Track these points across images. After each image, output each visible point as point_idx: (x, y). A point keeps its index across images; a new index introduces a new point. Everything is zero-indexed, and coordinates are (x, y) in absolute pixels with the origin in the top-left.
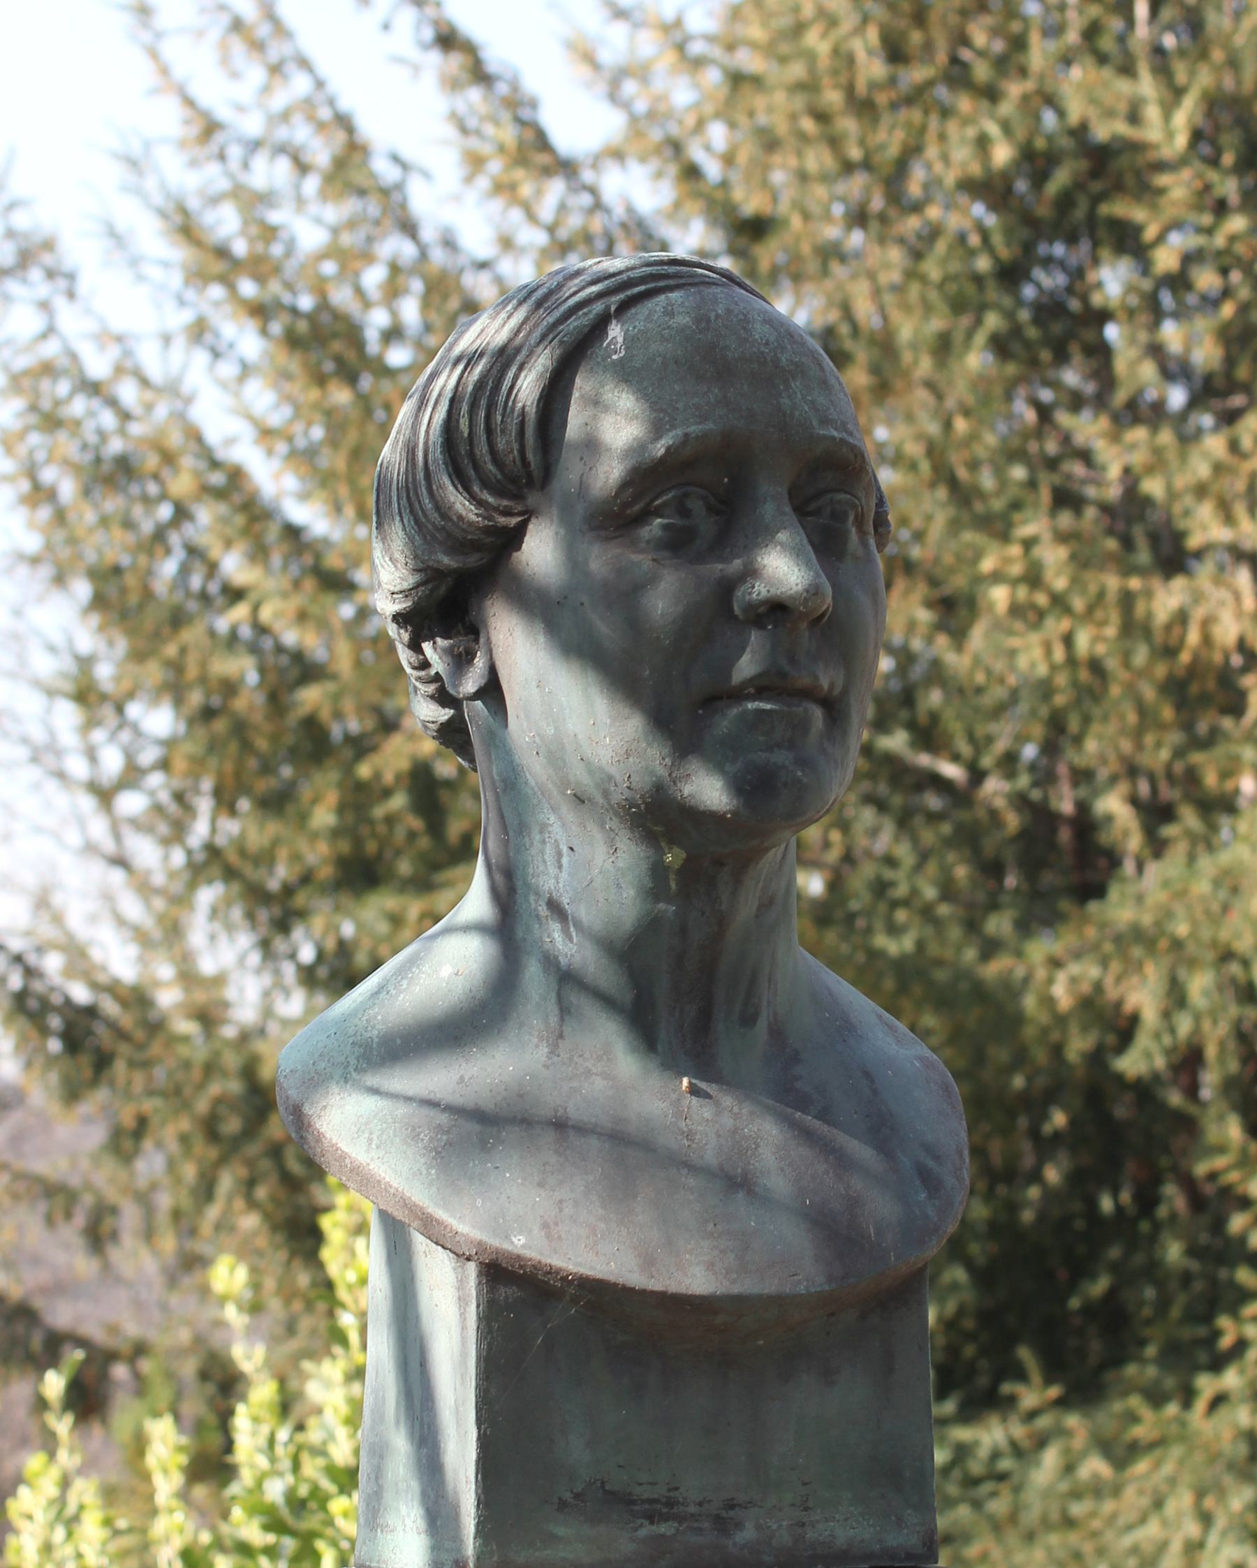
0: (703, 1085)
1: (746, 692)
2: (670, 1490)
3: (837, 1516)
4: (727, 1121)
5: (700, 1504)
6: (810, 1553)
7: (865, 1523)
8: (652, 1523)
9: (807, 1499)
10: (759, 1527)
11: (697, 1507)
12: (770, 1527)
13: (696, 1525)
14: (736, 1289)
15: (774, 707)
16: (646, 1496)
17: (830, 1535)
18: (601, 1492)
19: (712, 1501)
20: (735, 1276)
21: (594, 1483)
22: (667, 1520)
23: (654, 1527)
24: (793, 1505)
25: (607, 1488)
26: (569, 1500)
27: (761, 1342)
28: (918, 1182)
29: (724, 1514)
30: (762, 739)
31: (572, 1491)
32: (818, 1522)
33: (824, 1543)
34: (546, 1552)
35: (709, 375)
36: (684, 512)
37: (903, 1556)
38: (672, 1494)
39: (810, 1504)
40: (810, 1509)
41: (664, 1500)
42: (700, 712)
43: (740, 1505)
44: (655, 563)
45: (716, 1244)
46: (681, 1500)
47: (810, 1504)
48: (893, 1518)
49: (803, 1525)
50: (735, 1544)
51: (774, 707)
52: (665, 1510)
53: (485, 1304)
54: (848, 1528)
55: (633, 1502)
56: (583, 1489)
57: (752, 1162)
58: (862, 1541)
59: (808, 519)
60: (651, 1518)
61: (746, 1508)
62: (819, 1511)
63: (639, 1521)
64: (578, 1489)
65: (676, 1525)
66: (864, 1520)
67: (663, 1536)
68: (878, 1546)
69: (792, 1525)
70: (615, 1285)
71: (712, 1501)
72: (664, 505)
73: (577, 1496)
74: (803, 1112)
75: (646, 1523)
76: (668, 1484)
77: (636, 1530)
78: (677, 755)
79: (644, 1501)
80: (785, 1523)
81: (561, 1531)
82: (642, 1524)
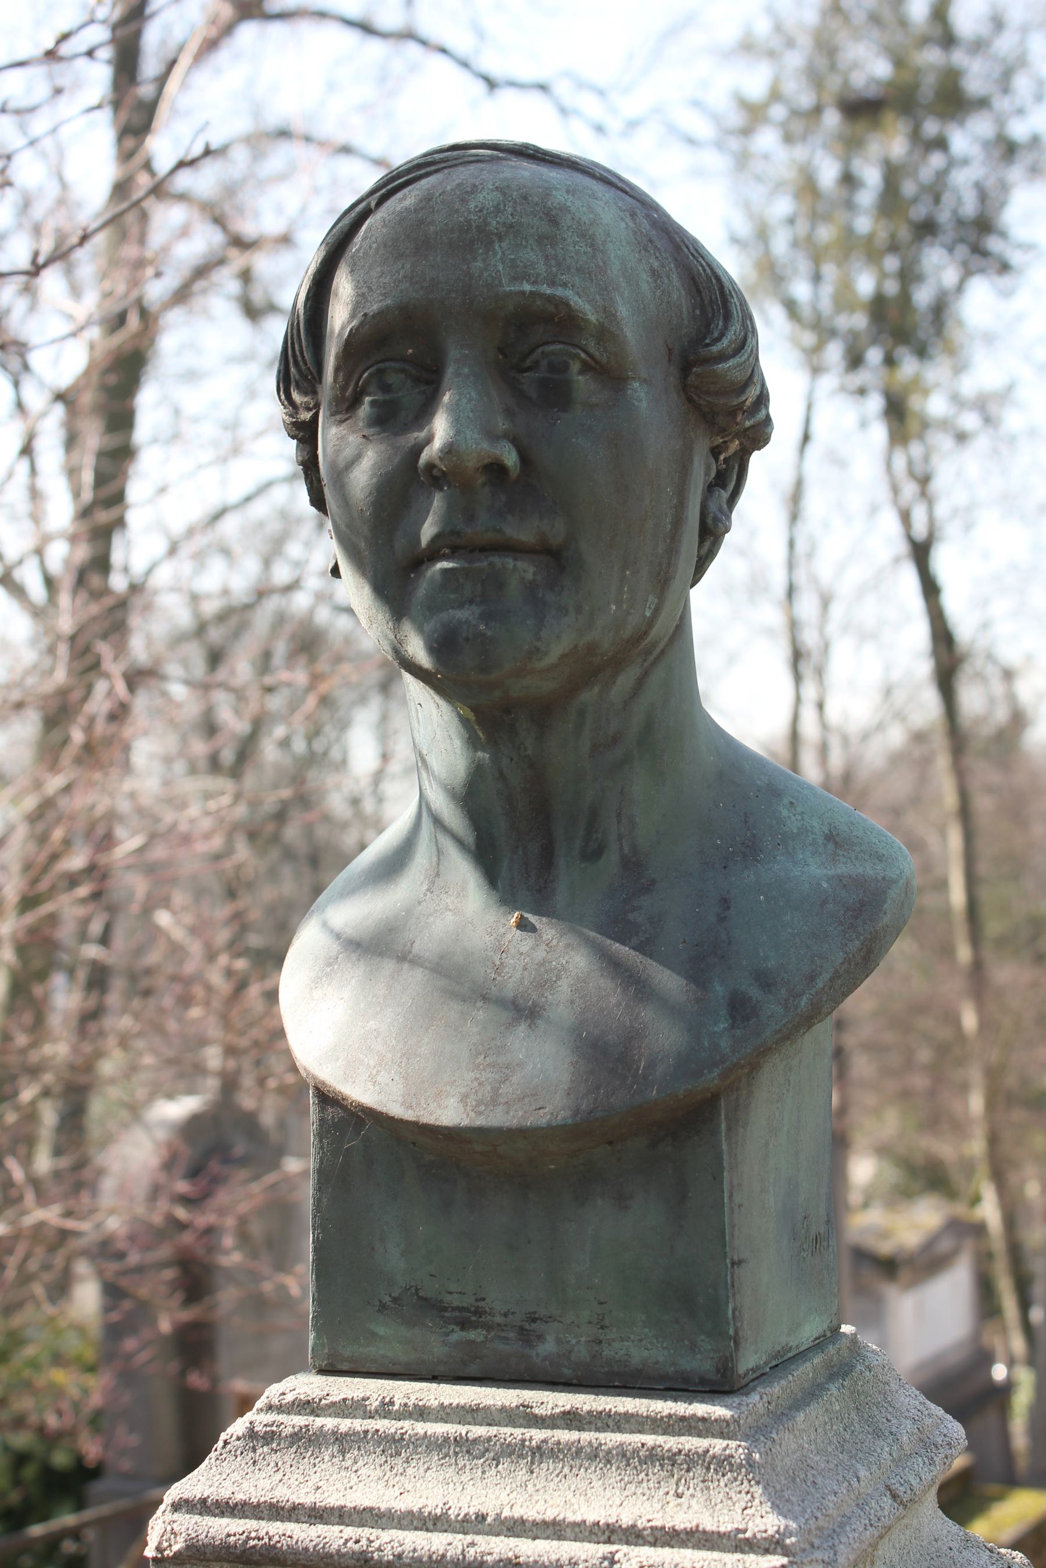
0: (532, 918)
1: (442, 552)
2: (477, 1300)
3: (632, 1337)
4: (540, 954)
5: (505, 1315)
6: (607, 1369)
7: (659, 1345)
8: (463, 1329)
9: (603, 1317)
10: (559, 1341)
11: (502, 1317)
12: (569, 1341)
13: (503, 1334)
14: (480, 1122)
15: (455, 565)
16: (456, 1304)
17: (625, 1355)
18: (415, 1297)
19: (516, 1313)
20: (483, 1108)
21: (409, 1289)
22: (476, 1328)
23: (464, 1334)
24: (590, 1323)
25: (420, 1294)
26: (388, 1303)
27: (553, 1167)
28: (723, 1012)
29: (527, 1327)
30: (452, 596)
31: (390, 1296)
32: (614, 1340)
33: (620, 1361)
34: (369, 1349)
35: (408, 252)
36: (386, 388)
37: (697, 1381)
38: (481, 1304)
39: (607, 1322)
40: (607, 1327)
41: (473, 1309)
42: (412, 575)
43: (541, 1319)
44: (364, 440)
45: (478, 1076)
46: (488, 1310)
47: (607, 1322)
48: (686, 1342)
49: (600, 1342)
50: (538, 1355)
51: (455, 565)
52: (474, 1318)
53: (318, 1123)
54: (643, 1349)
55: (445, 1309)
56: (399, 1294)
57: (546, 995)
58: (657, 1363)
59: (525, 375)
60: (464, 1325)
61: (546, 1322)
62: (614, 1330)
63: (451, 1327)
64: (395, 1294)
65: (484, 1332)
66: (658, 1342)
67: (473, 1342)
68: (672, 1369)
69: (589, 1341)
70: (381, 1113)
71: (516, 1313)
72: (367, 382)
73: (395, 1300)
74: (623, 943)
75: (457, 1328)
76: (475, 1294)
77: (447, 1335)
78: (394, 618)
79: (454, 1309)
80: (583, 1339)
81: (381, 1331)
82: (453, 1329)
